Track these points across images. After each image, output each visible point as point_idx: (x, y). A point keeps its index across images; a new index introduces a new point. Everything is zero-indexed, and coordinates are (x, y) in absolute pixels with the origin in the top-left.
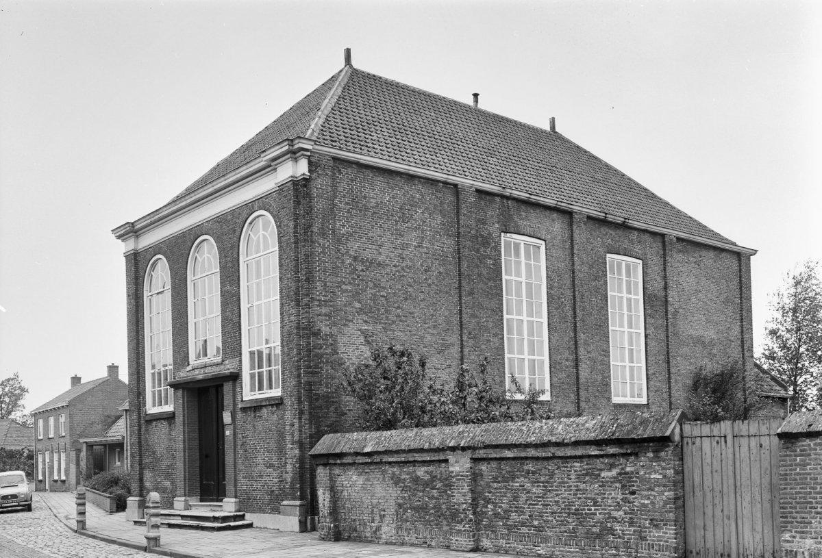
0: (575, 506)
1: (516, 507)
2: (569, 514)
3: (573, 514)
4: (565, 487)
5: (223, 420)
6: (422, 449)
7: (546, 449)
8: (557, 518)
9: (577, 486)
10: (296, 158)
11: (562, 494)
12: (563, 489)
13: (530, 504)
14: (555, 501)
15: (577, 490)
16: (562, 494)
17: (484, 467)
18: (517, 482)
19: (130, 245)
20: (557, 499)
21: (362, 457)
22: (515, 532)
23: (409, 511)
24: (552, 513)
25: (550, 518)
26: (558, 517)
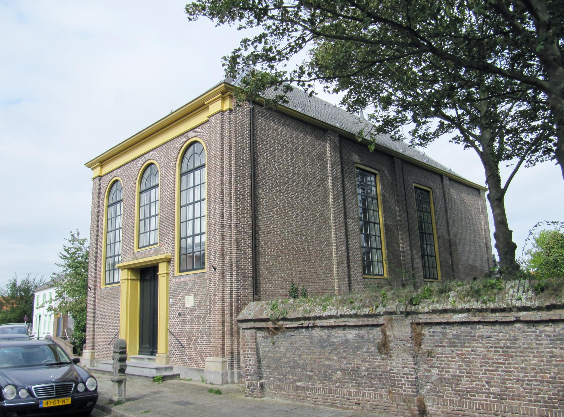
0: (550, 373)
1: (467, 373)
2: (542, 382)
3: (548, 382)
4: (533, 353)
5: (492, 252)
6: (321, 316)
7: (442, 316)
8: (525, 386)
9: (552, 352)
10: (224, 98)
11: (530, 360)
12: (531, 355)
13: (486, 370)
14: (522, 368)
15: (551, 357)
16: (530, 360)
17: (426, 331)
18: (468, 347)
19: (97, 172)
20: (523, 365)
21: (290, 323)
22: (469, 399)
23: (338, 372)
24: (518, 380)
25: (515, 386)
26: (527, 384)
